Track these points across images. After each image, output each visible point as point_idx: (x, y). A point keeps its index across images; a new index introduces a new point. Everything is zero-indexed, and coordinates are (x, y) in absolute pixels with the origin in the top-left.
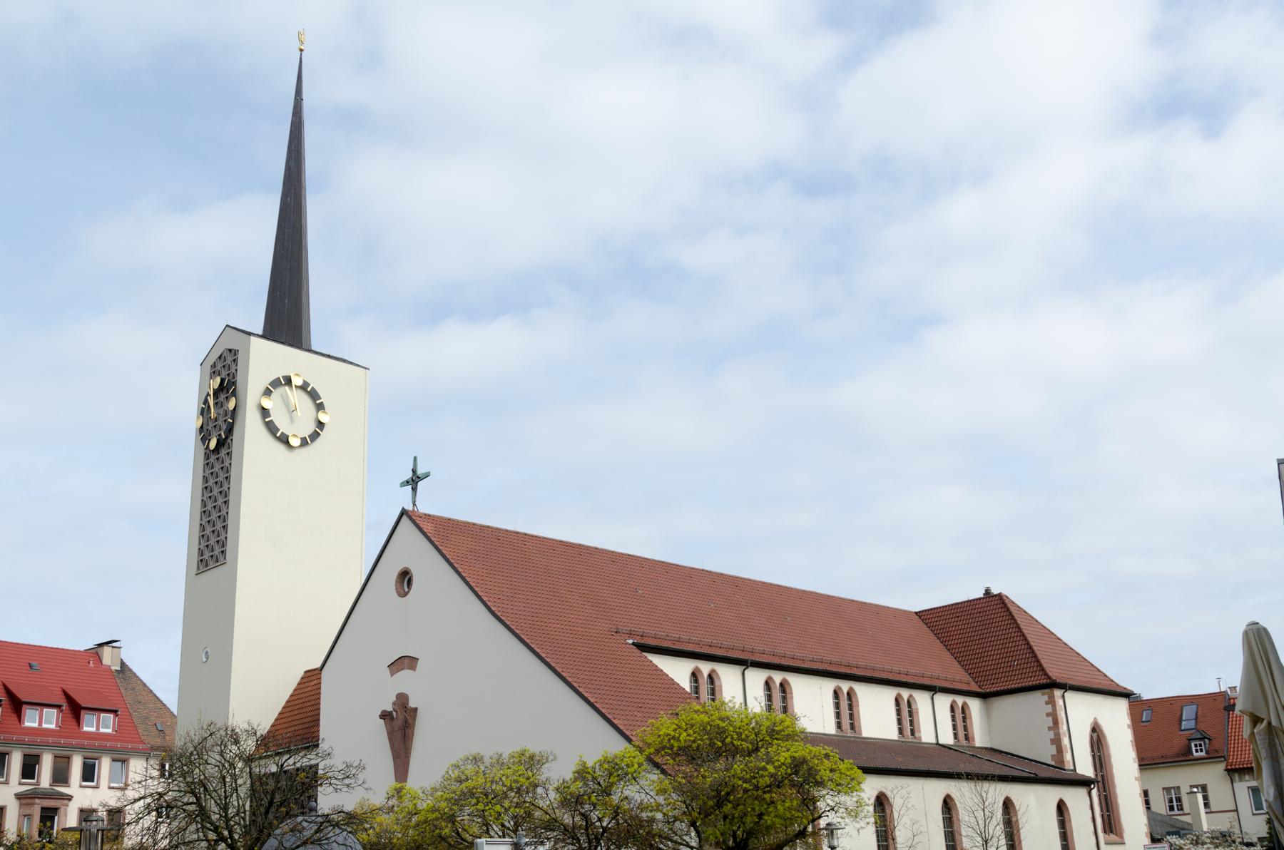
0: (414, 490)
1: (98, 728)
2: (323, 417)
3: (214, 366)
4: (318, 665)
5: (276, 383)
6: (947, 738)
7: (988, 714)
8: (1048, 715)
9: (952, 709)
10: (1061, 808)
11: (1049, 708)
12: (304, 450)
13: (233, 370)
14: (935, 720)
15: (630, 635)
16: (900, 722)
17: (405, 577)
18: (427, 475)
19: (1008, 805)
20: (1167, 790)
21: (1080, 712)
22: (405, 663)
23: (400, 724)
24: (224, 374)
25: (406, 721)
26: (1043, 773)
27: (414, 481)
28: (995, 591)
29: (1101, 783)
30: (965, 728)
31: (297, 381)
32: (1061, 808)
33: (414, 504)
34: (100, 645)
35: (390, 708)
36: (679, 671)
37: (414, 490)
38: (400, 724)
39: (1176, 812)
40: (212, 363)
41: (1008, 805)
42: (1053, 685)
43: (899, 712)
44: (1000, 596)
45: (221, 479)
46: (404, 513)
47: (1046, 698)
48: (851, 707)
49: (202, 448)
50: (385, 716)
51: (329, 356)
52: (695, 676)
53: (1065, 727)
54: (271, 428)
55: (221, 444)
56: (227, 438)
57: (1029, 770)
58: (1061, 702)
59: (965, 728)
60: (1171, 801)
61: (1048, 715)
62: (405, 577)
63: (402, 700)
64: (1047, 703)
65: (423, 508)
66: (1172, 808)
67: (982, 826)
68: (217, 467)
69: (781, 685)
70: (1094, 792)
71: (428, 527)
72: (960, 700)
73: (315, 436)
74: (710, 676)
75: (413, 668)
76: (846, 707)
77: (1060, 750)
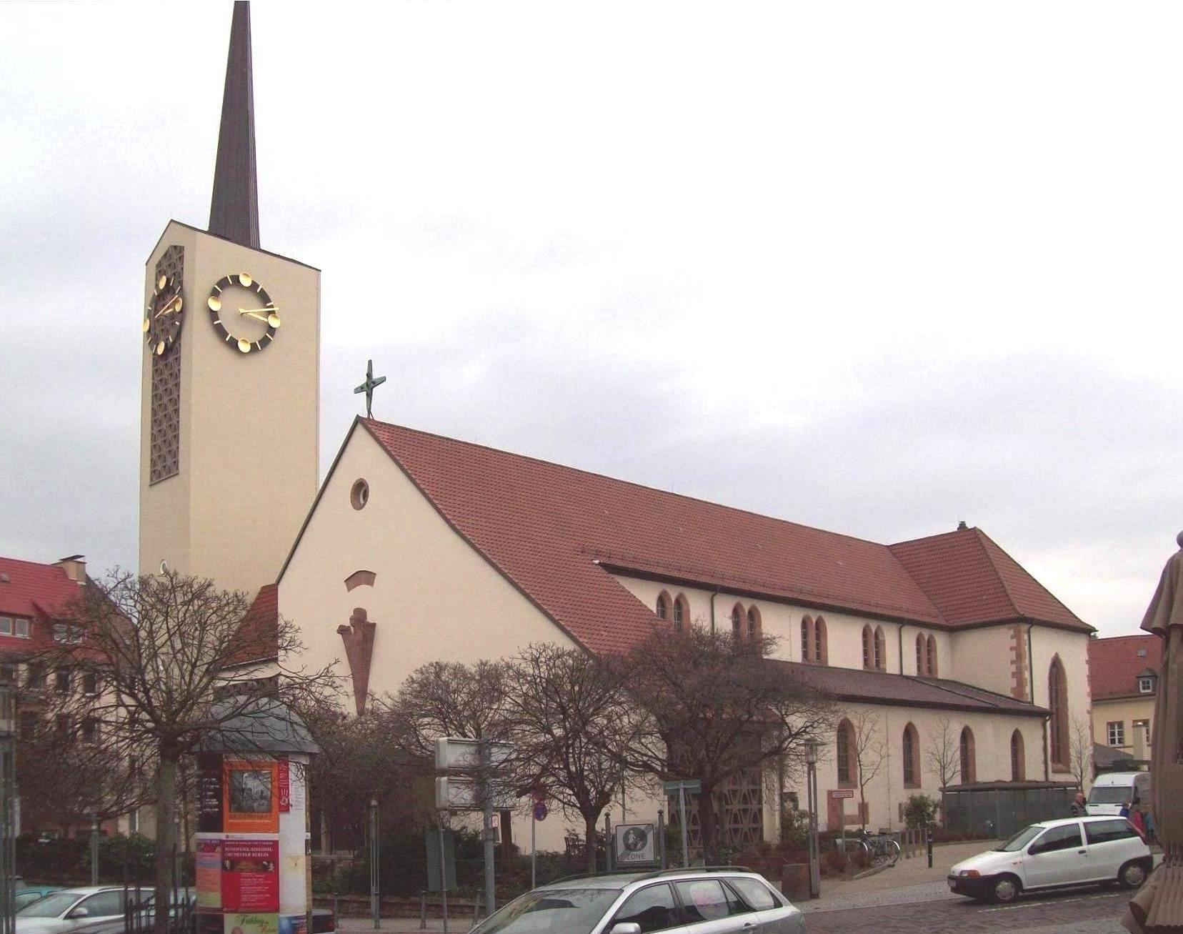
0: (369, 396)
3: (159, 265)
4: (273, 581)
5: (223, 283)
6: (911, 669)
7: (952, 646)
8: (1012, 649)
10: (1016, 739)
14: (901, 655)
15: (598, 554)
17: (360, 491)
18: (383, 380)
19: (966, 736)
20: (1111, 725)
21: (1044, 647)
22: (361, 578)
23: (360, 637)
24: (170, 272)
26: (1002, 705)
27: (369, 386)
28: (969, 526)
29: (1055, 715)
30: (929, 661)
31: (246, 282)
33: (369, 412)
35: (347, 623)
36: (647, 596)
37: (369, 396)
38: (360, 637)
42: (1022, 620)
44: (975, 531)
46: (359, 420)
47: (1012, 632)
49: (150, 354)
50: (342, 630)
52: (662, 600)
53: (1027, 661)
54: (220, 331)
55: (168, 349)
56: (174, 342)
57: (989, 702)
58: (1026, 637)
59: (929, 661)
60: (1113, 734)
61: (1012, 649)
62: (360, 491)
65: (378, 416)
66: (1113, 741)
67: (941, 747)
68: (166, 375)
69: (750, 612)
70: (1048, 723)
72: (926, 634)
73: (265, 342)
74: (678, 601)
75: (371, 583)
76: (814, 636)
77: (1021, 683)
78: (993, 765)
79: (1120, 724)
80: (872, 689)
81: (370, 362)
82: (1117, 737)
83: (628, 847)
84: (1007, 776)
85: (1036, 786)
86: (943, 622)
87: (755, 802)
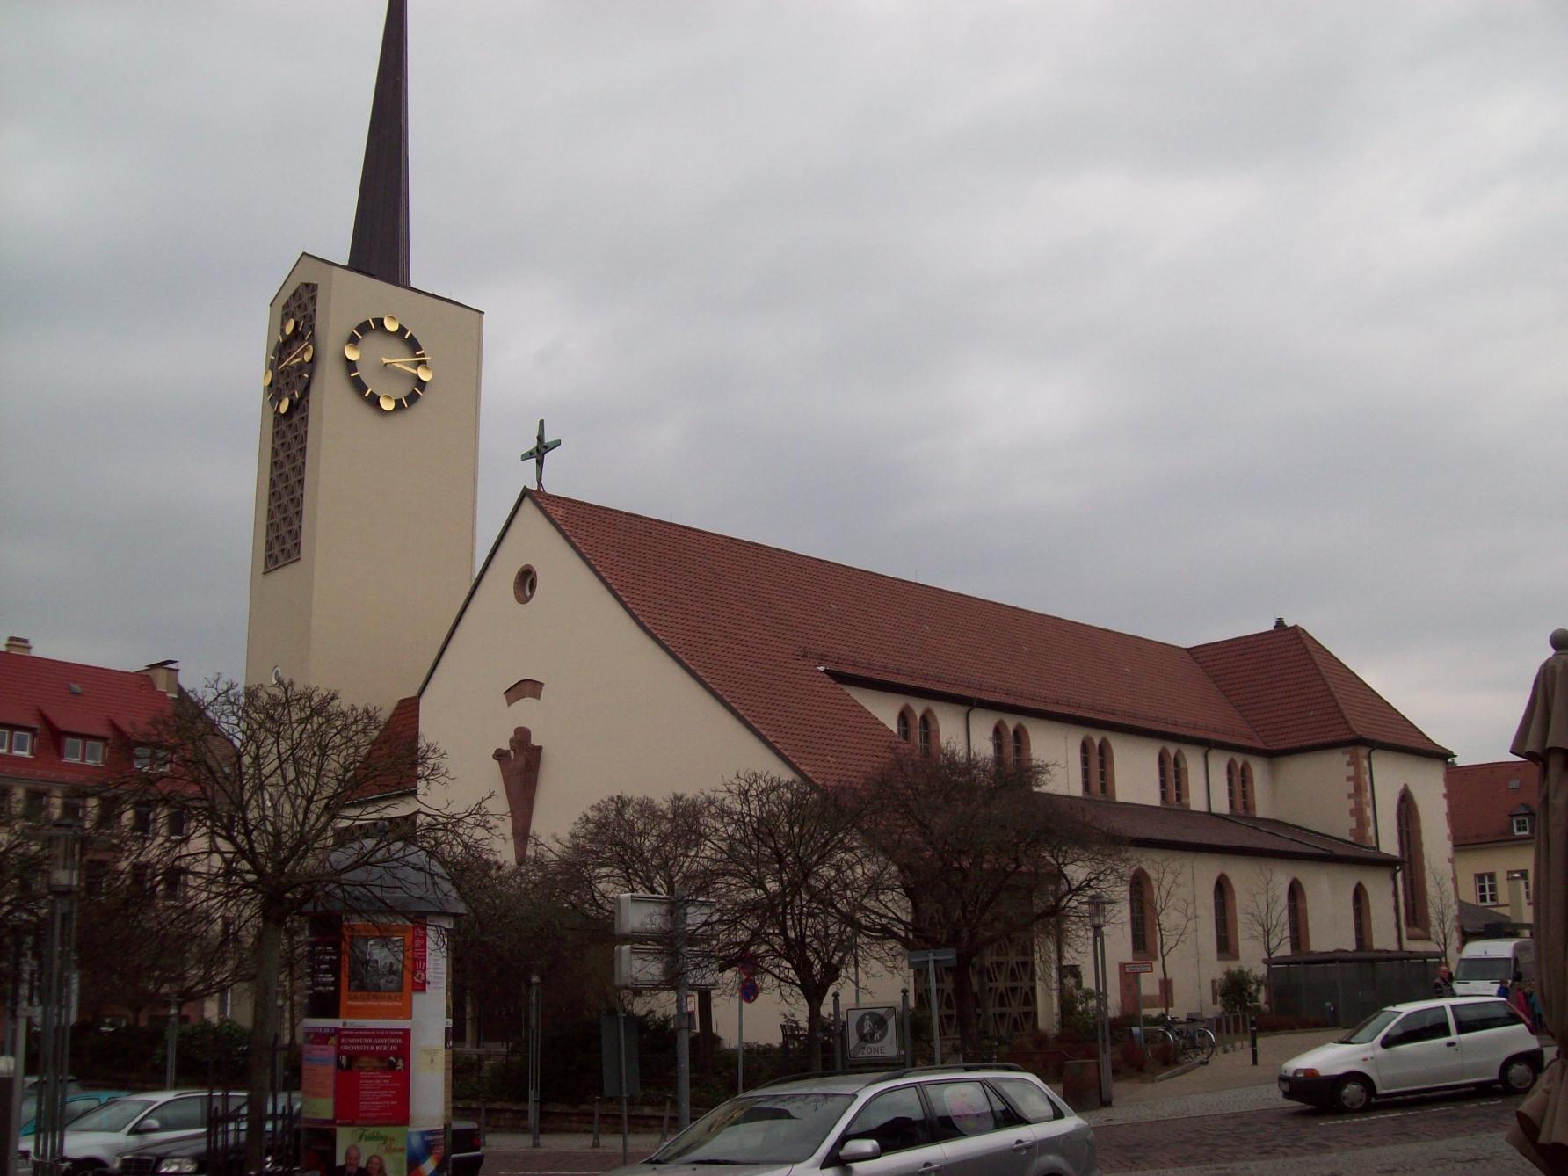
0: (540, 463)
1: (10, 750)
3: (286, 306)
4: (414, 693)
5: (364, 328)
6: (1221, 805)
7: (1273, 775)
8: (1349, 779)
9: (1230, 771)
10: (1359, 896)
11: (1351, 771)
12: (399, 416)
13: (310, 311)
14: (1207, 785)
15: (823, 659)
16: (1163, 784)
17: (526, 580)
18: (557, 444)
19: (1295, 891)
20: (1480, 877)
22: (526, 689)
23: (522, 764)
25: (528, 763)
26: (1339, 851)
27: (540, 451)
28: (1289, 623)
29: (1407, 865)
30: (1244, 795)
31: (392, 327)
32: (1359, 896)
33: (539, 483)
34: (153, 667)
35: (506, 746)
36: (885, 711)
37: (540, 463)
38: (522, 764)
39: (1489, 902)
40: (283, 302)
41: (1295, 891)
43: (1162, 772)
44: (1296, 630)
45: (294, 451)
46: (526, 493)
47: (1347, 758)
48: (1102, 763)
50: (500, 755)
51: (433, 296)
52: (904, 717)
53: (1369, 795)
54: (359, 385)
56: (301, 398)
57: (1322, 847)
58: (1366, 764)
59: (1244, 795)
60: (1482, 889)
61: (1349, 779)
62: (526, 580)
63: (522, 736)
64: (1349, 764)
65: (551, 488)
66: (1483, 899)
67: (1263, 907)
69: (1016, 732)
70: (1399, 875)
71: (557, 513)
72: (1239, 760)
73: (413, 398)
74: (924, 718)
75: (537, 695)
76: (1097, 763)
78: (1331, 930)
79: (1492, 876)
80: (1174, 832)
81: (542, 422)
82: (1488, 893)
83: (862, 1038)
84: (1350, 944)
85: (1387, 957)
86: (1260, 745)
87: (1026, 978)
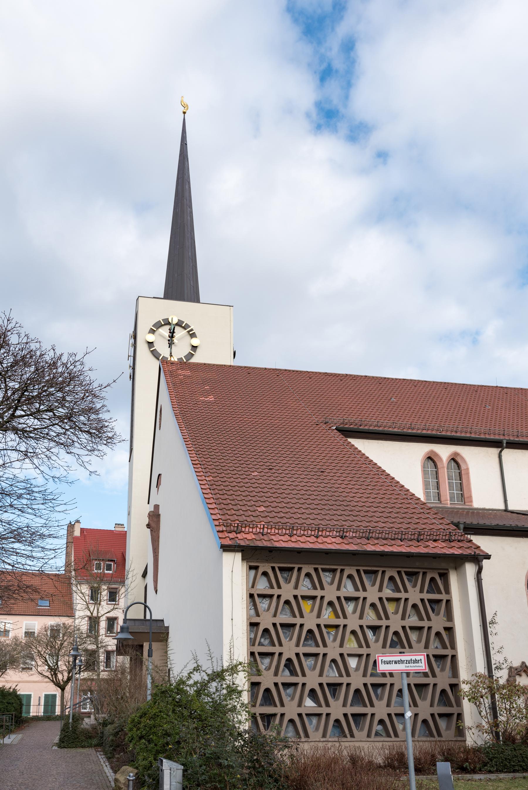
2: (195, 342)
